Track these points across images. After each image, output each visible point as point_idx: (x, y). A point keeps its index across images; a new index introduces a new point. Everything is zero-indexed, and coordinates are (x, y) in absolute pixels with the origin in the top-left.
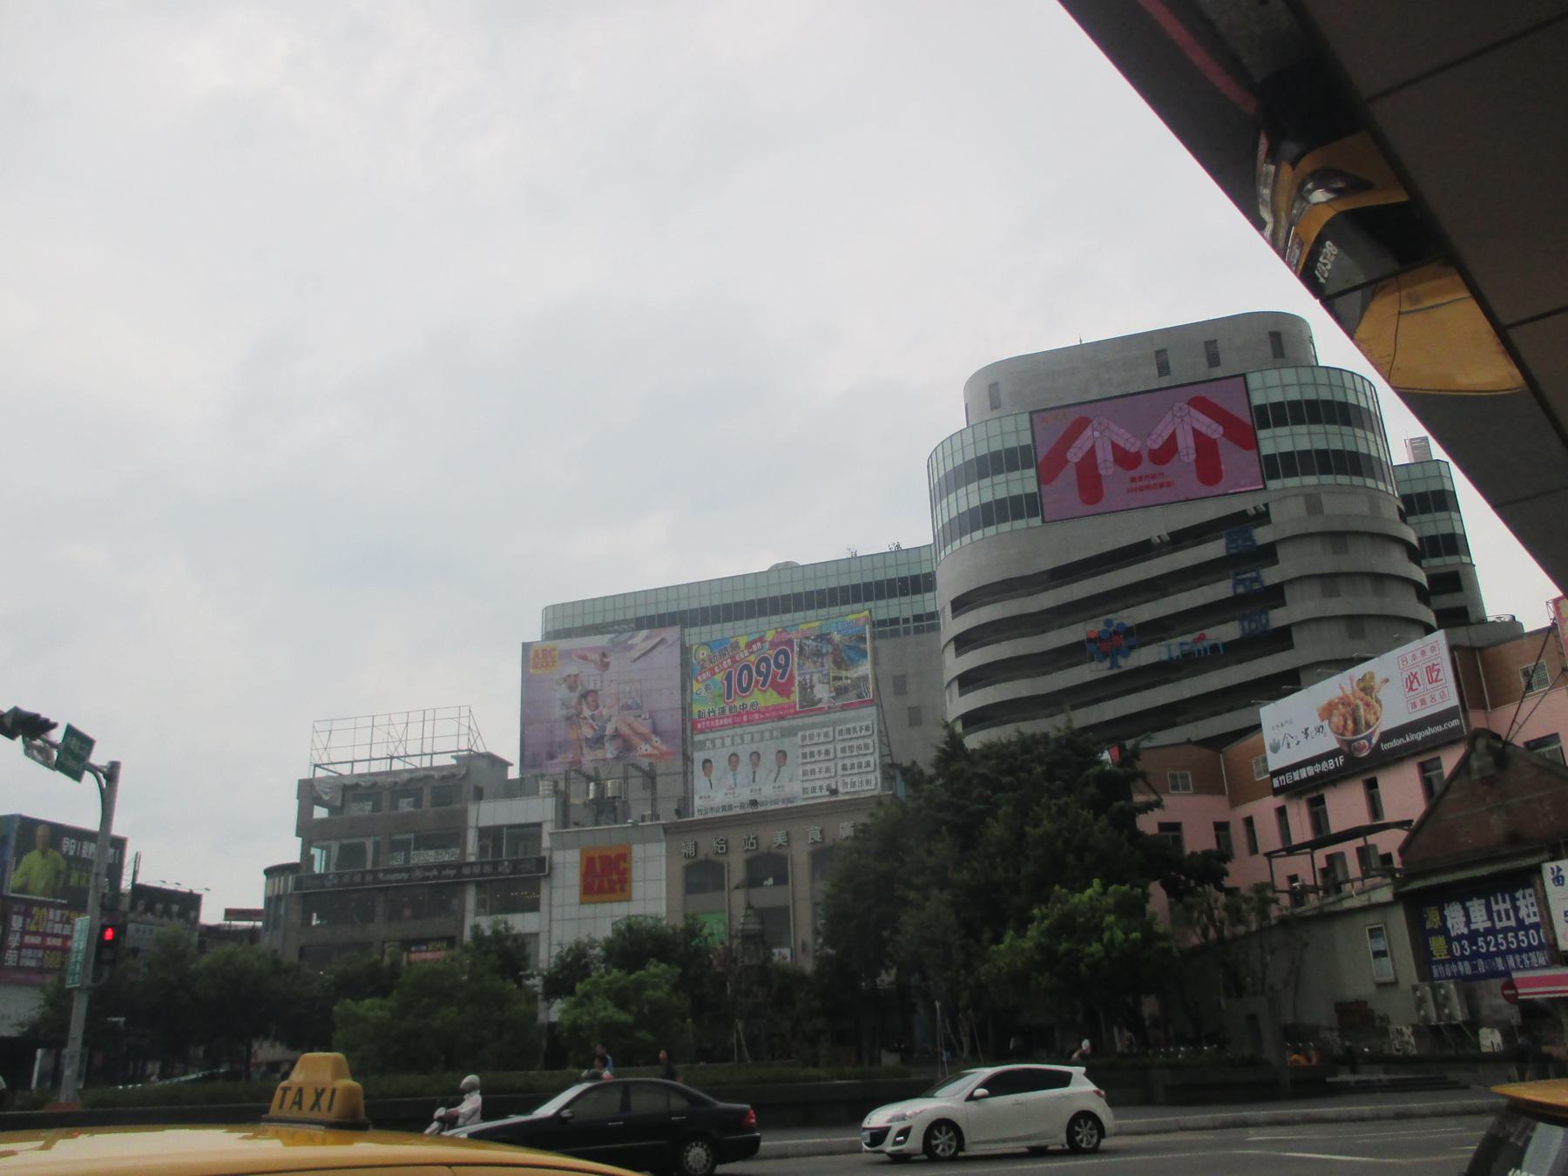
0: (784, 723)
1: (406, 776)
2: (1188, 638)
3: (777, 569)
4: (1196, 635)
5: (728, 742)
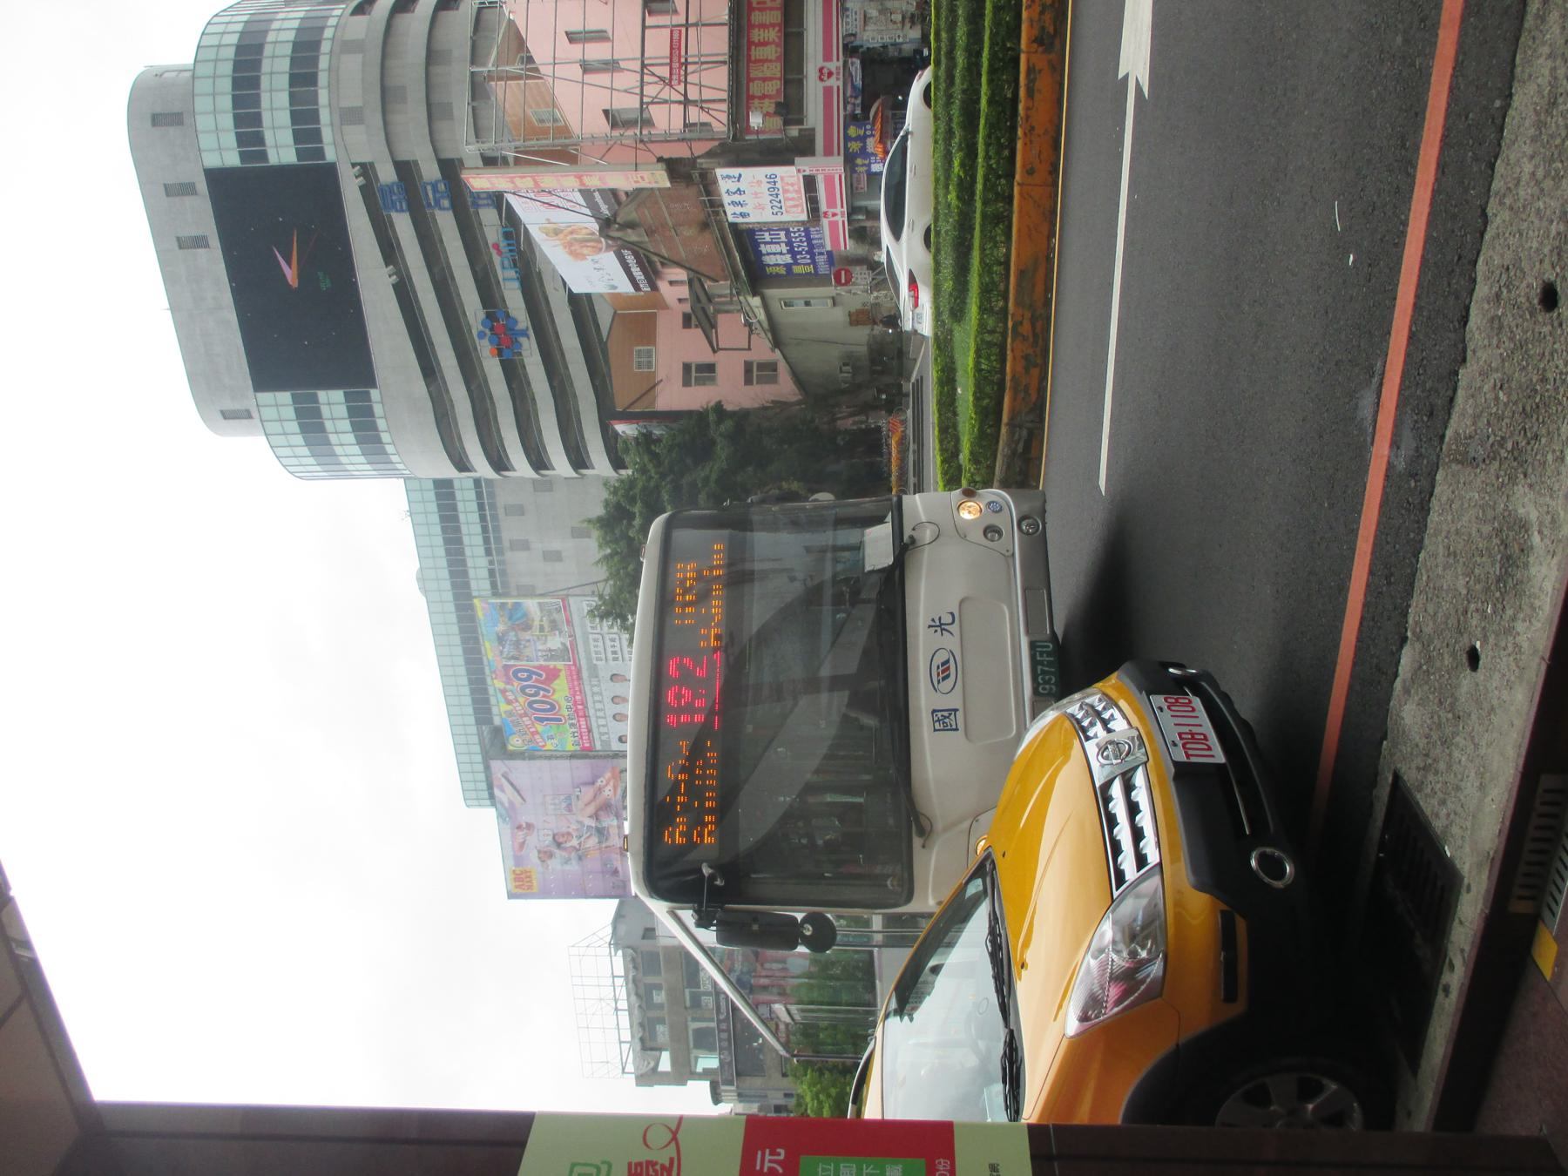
0: (585, 674)
1: (633, 998)
2: (497, 259)
3: (424, 590)
4: (494, 252)
5: (602, 722)
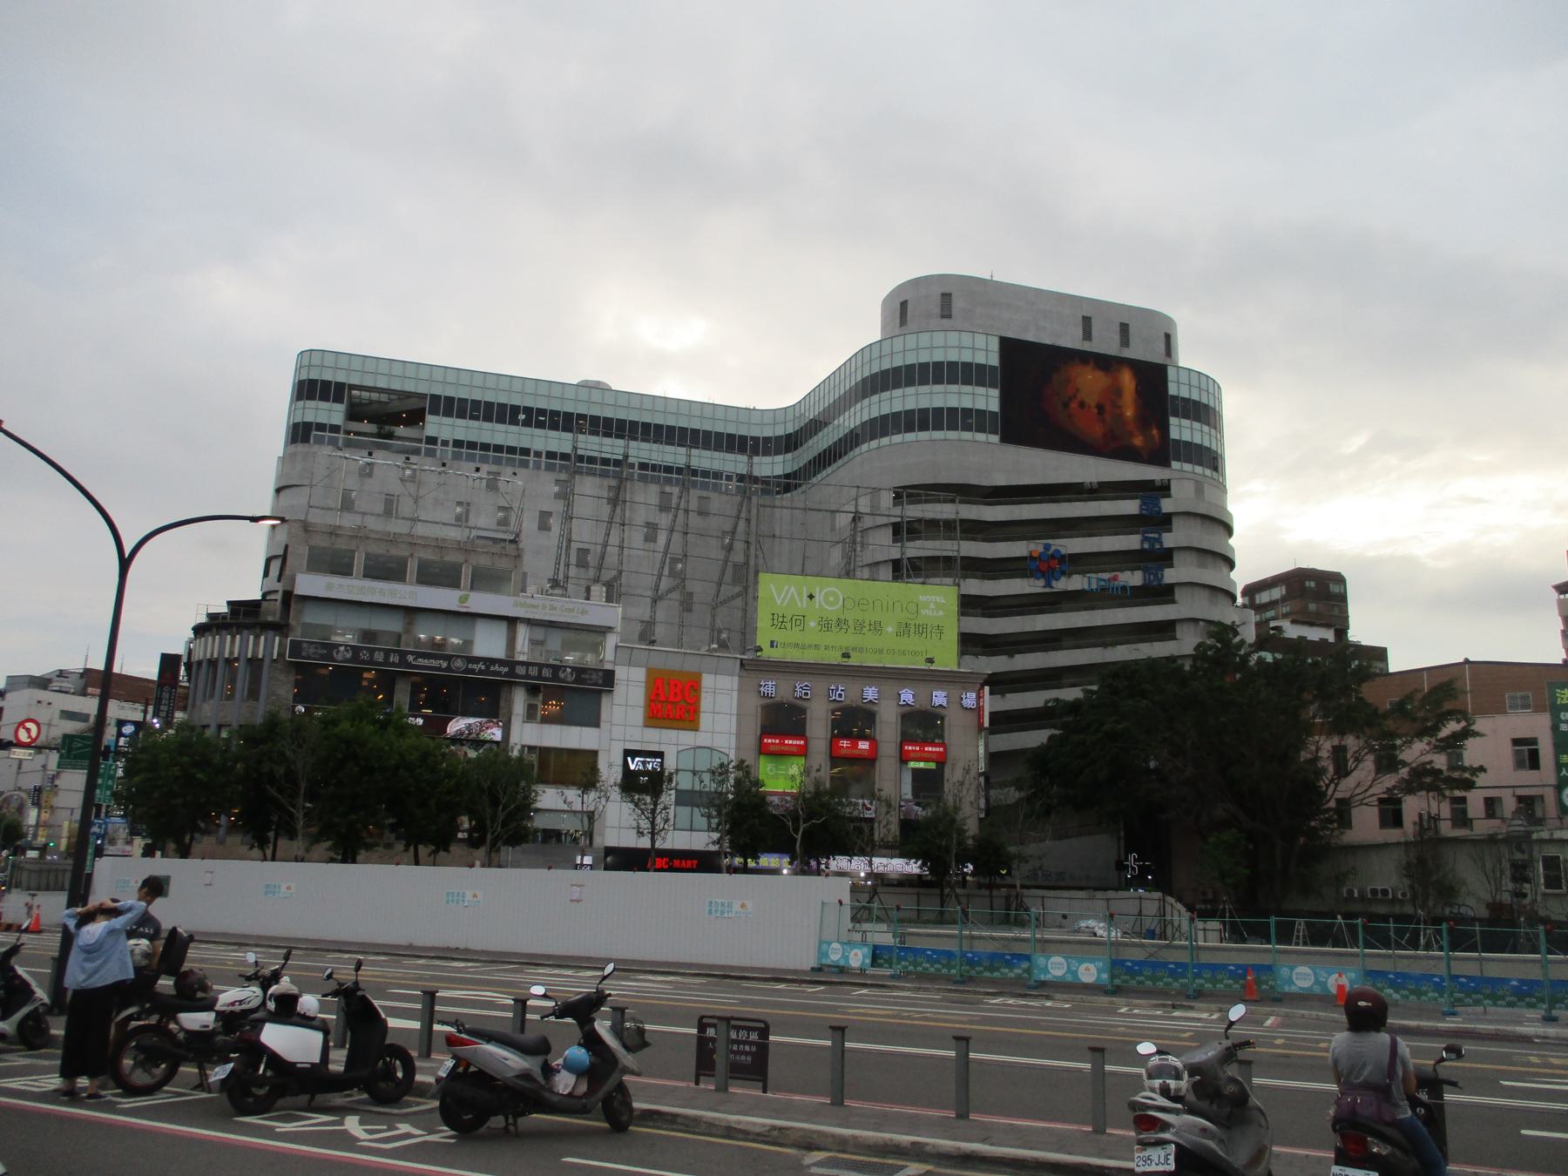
2: (1106, 576)
3: (586, 386)
